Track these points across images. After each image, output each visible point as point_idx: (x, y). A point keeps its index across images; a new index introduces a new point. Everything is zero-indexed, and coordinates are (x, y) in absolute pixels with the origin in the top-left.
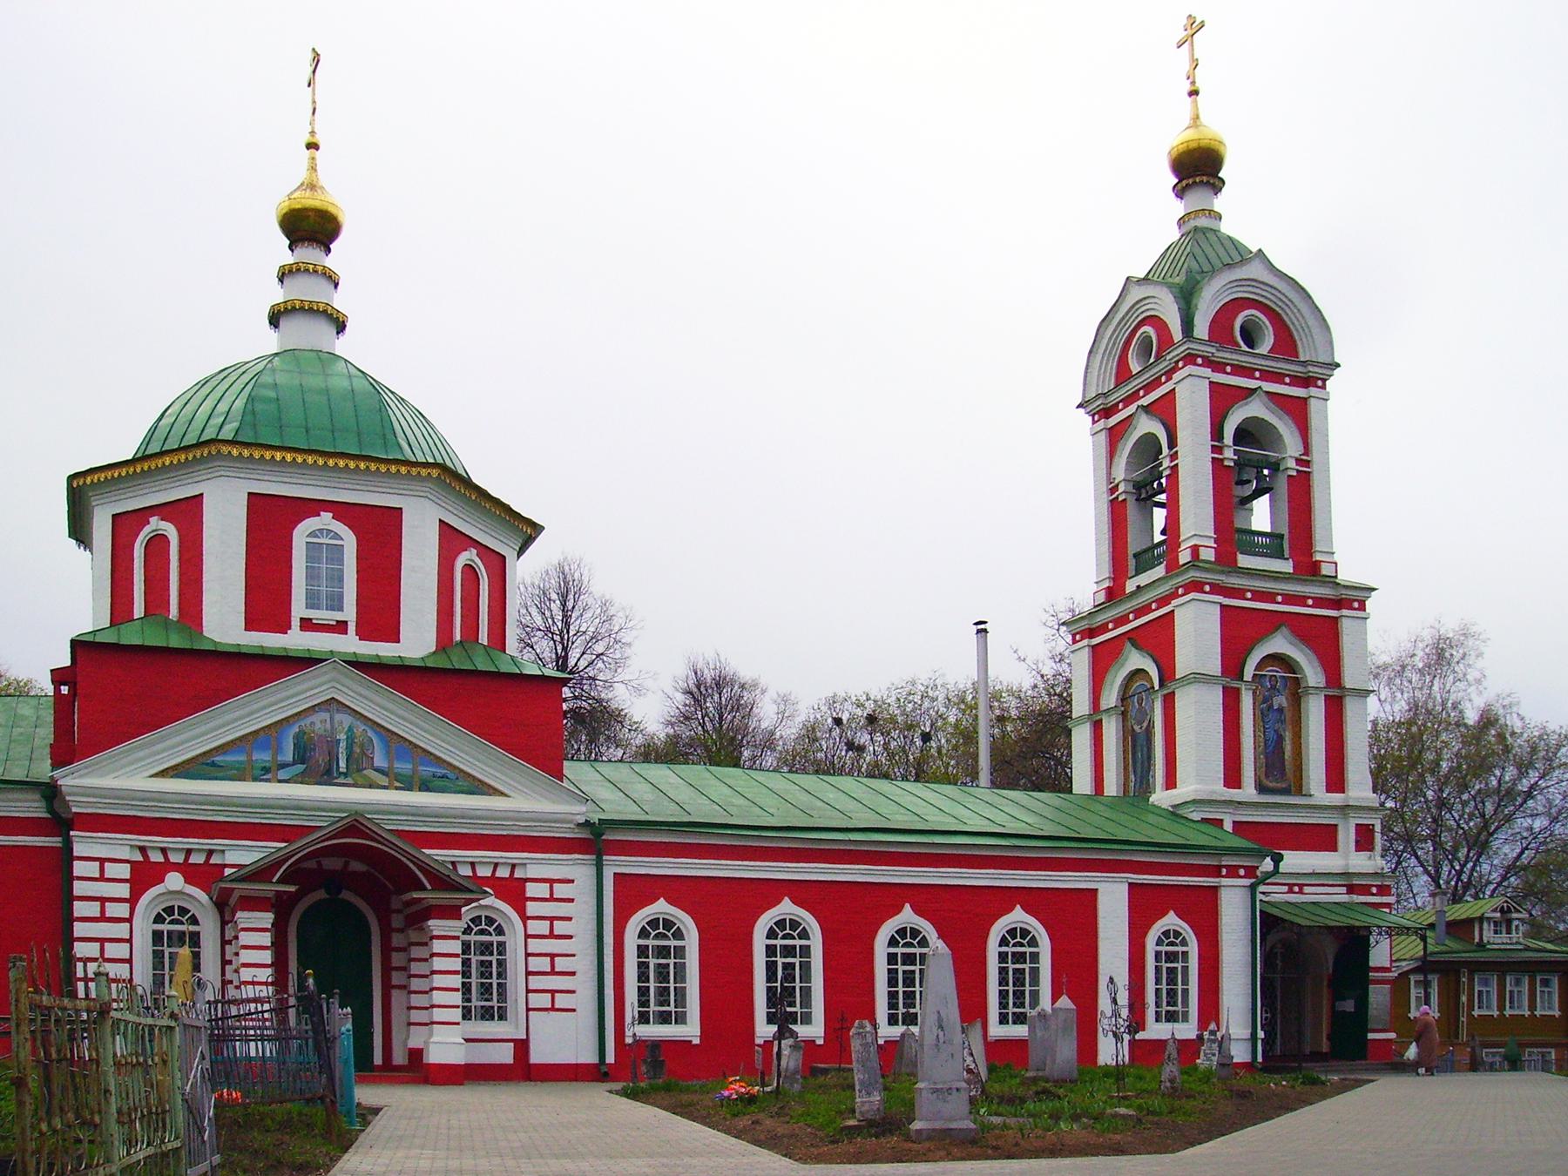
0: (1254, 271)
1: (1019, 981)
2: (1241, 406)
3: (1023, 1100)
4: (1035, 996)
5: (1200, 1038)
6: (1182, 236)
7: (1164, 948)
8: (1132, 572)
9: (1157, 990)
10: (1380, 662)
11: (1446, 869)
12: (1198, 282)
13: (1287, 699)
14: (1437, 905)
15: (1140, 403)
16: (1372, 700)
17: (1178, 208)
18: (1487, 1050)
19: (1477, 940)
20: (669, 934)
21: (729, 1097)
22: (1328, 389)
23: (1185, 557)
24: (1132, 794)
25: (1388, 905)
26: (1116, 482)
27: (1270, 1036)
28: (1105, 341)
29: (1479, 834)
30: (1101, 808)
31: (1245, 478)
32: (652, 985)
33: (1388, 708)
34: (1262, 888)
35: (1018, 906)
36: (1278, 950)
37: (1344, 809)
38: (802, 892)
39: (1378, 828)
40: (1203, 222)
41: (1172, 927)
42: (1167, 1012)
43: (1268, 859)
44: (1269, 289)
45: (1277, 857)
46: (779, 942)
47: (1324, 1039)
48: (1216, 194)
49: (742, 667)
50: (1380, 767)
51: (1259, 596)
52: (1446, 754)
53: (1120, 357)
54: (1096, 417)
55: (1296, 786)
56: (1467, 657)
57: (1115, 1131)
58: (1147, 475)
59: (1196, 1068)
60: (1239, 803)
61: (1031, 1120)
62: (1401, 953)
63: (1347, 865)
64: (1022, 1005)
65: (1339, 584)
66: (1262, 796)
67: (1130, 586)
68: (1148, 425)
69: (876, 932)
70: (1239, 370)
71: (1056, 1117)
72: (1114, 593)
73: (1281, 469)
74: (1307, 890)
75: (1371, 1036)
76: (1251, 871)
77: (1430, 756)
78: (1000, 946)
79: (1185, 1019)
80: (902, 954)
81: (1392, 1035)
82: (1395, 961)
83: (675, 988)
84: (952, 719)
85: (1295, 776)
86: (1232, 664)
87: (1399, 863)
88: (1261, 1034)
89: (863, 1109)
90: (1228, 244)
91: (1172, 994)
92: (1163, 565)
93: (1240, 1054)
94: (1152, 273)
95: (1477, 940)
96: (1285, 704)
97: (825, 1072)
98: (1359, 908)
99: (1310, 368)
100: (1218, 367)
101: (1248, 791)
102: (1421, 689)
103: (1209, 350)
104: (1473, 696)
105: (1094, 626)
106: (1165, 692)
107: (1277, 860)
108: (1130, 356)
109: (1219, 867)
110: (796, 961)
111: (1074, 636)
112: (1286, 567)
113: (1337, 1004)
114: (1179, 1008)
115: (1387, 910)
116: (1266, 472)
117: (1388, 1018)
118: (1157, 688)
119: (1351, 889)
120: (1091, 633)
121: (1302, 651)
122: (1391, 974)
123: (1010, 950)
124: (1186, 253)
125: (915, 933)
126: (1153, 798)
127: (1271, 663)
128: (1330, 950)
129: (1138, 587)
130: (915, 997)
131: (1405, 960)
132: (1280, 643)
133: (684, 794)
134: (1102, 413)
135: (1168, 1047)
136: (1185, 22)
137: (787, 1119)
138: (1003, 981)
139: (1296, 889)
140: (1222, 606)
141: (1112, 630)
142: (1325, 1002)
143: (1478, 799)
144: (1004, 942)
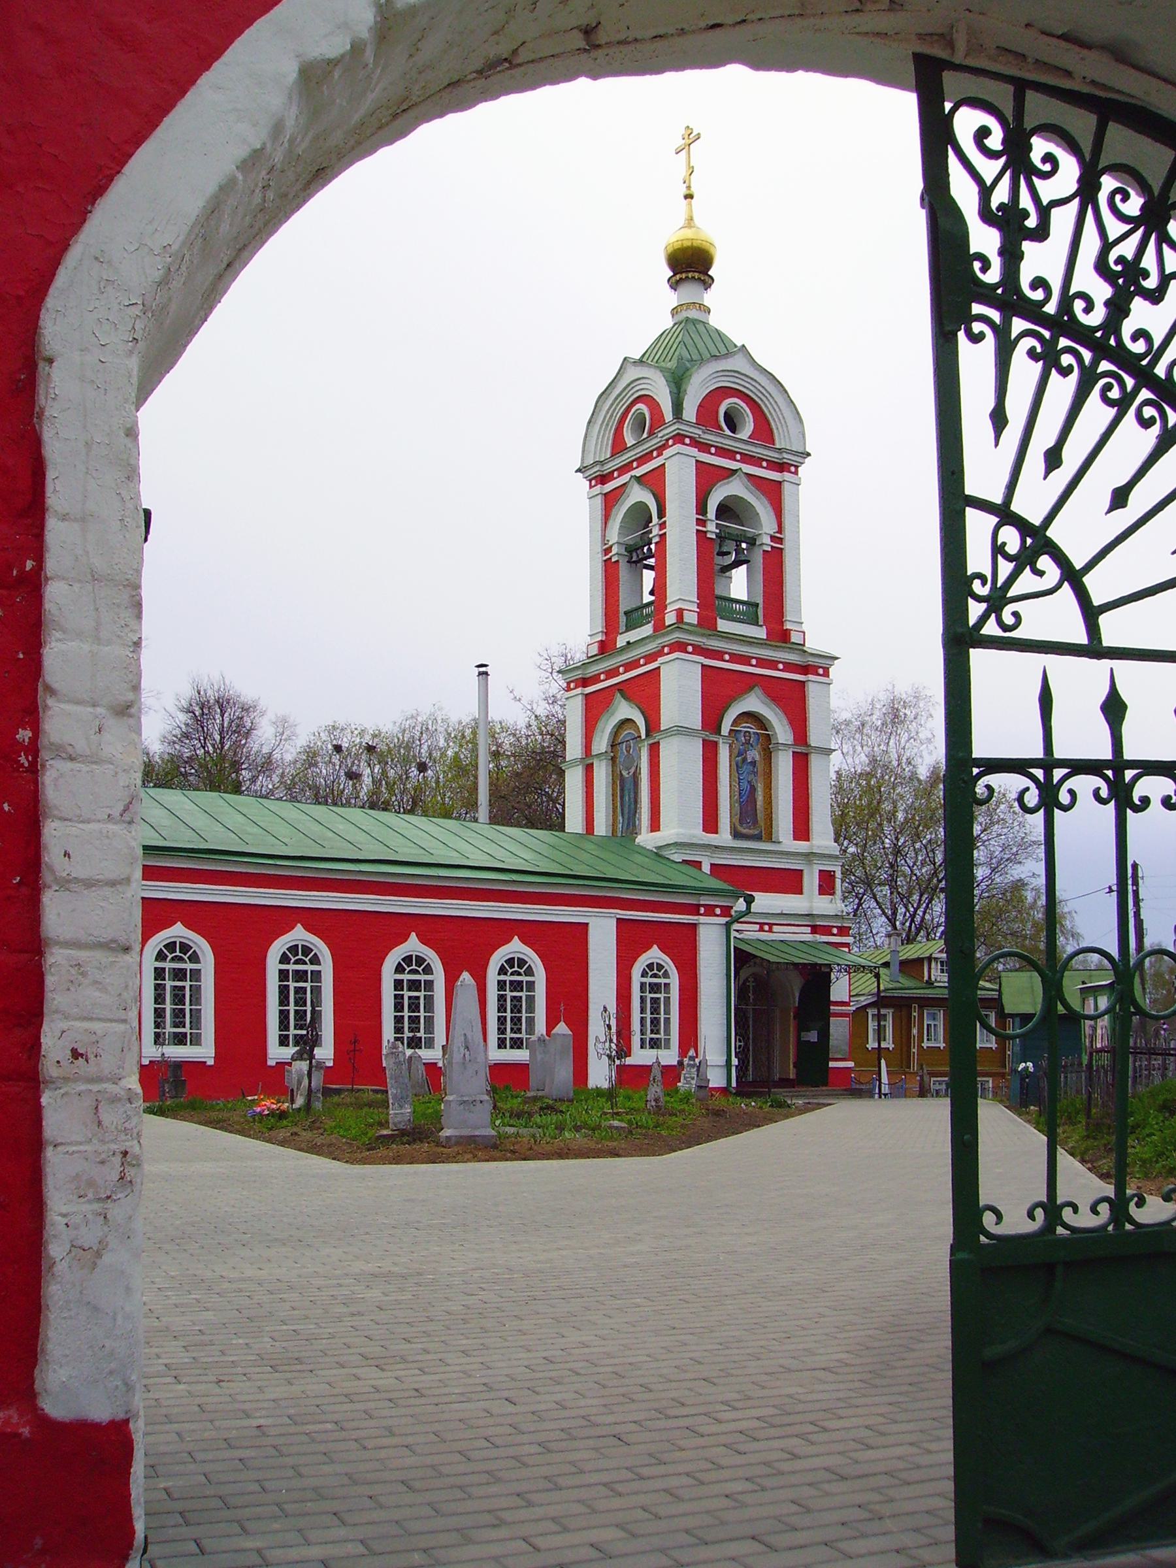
0: (737, 363)
1: (516, 1008)
2: (725, 484)
3: (530, 1115)
4: (531, 1021)
5: (681, 1063)
6: (675, 324)
7: (648, 980)
8: (622, 628)
9: (642, 1018)
10: (840, 720)
11: (901, 910)
12: (688, 370)
13: (760, 754)
14: (892, 945)
15: (633, 473)
16: (836, 758)
17: (672, 299)
18: (935, 1079)
19: (926, 978)
20: (186, 957)
21: (260, 1113)
22: (800, 475)
23: (670, 619)
24: (619, 835)
25: (847, 945)
26: (610, 543)
27: (743, 1063)
28: (603, 413)
29: (930, 880)
30: (593, 846)
31: (725, 549)
32: (168, 1006)
33: (850, 761)
34: (736, 926)
35: (516, 937)
36: (751, 984)
37: (809, 856)
38: (314, 919)
39: (838, 875)
40: (693, 314)
41: (655, 961)
42: (651, 1039)
43: (742, 900)
44: (749, 380)
45: (748, 899)
46: (291, 967)
47: (791, 1066)
48: (706, 289)
49: (244, 688)
50: (843, 815)
51: (736, 658)
52: (901, 806)
53: (616, 430)
54: (593, 482)
55: (768, 834)
56: (919, 717)
57: (612, 1139)
58: (638, 539)
59: (677, 1090)
60: (716, 847)
61: (540, 1130)
62: (860, 988)
63: (811, 907)
64: (519, 1031)
65: (805, 652)
66: (736, 842)
67: (621, 641)
68: (639, 495)
69: (384, 959)
70: (723, 452)
71: (560, 1128)
72: (606, 647)
73: (757, 543)
74: (775, 928)
75: (832, 1064)
76: (726, 911)
77: (887, 806)
78: (499, 974)
79: (667, 1047)
80: (408, 980)
81: (851, 1064)
82: (853, 996)
83: (191, 1010)
84: (450, 753)
85: (765, 824)
86: (712, 721)
87: (860, 904)
88: (735, 1061)
89: (396, 1120)
90: (715, 336)
91: (655, 1022)
92: (651, 625)
93: (716, 1079)
94: (647, 355)
95: (926, 978)
96: (757, 758)
97: (338, 1092)
98: (820, 947)
99: (785, 455)
100: (704, 447)
101: (724, 836)
102: (879, 745)
103: (697, 432)
104: (925, 754)
105: (588, 676)
106: (652, 741)
107: (749, 900)
108: (625, 429)
109: (699, 906)
110: (308, 985)
111: (568, 683)
112: (761, 633)
113: (803, 1034)
114: (662, 1036)
115: (846, 950)
116: (744, 545)
117: (847, 1048)
118: (643, 737)
119: (815, 929)
120: (585, 682)
121: (773, 710)
122: (849, 1008)
123: (508, 978)
124: (678, 341)
125: (420, 960)
126: (640, 839)
127: (745, 719)
128: (795, 985)
129: (628, 643)
130: (419, 1021)
131: (863, 995)
132: (754, 702)
133: (201, 822)
134: (599, 478)
135: (653, 1070)
136: (683, 131)
137: (321, 1131)
138: (502, 1008)
139: (766, 928)
140: (703, 666)
141: (603, 681)
142: (791, 1029)
143: (929, 848)
144: (502, 971)
